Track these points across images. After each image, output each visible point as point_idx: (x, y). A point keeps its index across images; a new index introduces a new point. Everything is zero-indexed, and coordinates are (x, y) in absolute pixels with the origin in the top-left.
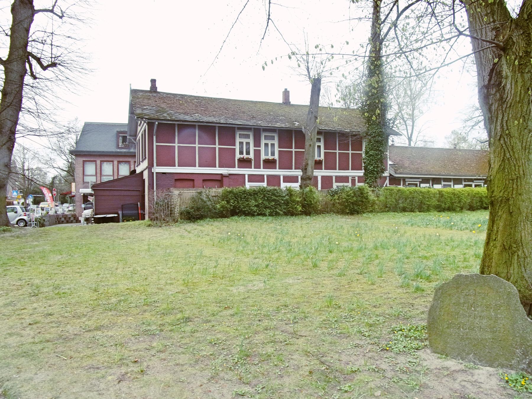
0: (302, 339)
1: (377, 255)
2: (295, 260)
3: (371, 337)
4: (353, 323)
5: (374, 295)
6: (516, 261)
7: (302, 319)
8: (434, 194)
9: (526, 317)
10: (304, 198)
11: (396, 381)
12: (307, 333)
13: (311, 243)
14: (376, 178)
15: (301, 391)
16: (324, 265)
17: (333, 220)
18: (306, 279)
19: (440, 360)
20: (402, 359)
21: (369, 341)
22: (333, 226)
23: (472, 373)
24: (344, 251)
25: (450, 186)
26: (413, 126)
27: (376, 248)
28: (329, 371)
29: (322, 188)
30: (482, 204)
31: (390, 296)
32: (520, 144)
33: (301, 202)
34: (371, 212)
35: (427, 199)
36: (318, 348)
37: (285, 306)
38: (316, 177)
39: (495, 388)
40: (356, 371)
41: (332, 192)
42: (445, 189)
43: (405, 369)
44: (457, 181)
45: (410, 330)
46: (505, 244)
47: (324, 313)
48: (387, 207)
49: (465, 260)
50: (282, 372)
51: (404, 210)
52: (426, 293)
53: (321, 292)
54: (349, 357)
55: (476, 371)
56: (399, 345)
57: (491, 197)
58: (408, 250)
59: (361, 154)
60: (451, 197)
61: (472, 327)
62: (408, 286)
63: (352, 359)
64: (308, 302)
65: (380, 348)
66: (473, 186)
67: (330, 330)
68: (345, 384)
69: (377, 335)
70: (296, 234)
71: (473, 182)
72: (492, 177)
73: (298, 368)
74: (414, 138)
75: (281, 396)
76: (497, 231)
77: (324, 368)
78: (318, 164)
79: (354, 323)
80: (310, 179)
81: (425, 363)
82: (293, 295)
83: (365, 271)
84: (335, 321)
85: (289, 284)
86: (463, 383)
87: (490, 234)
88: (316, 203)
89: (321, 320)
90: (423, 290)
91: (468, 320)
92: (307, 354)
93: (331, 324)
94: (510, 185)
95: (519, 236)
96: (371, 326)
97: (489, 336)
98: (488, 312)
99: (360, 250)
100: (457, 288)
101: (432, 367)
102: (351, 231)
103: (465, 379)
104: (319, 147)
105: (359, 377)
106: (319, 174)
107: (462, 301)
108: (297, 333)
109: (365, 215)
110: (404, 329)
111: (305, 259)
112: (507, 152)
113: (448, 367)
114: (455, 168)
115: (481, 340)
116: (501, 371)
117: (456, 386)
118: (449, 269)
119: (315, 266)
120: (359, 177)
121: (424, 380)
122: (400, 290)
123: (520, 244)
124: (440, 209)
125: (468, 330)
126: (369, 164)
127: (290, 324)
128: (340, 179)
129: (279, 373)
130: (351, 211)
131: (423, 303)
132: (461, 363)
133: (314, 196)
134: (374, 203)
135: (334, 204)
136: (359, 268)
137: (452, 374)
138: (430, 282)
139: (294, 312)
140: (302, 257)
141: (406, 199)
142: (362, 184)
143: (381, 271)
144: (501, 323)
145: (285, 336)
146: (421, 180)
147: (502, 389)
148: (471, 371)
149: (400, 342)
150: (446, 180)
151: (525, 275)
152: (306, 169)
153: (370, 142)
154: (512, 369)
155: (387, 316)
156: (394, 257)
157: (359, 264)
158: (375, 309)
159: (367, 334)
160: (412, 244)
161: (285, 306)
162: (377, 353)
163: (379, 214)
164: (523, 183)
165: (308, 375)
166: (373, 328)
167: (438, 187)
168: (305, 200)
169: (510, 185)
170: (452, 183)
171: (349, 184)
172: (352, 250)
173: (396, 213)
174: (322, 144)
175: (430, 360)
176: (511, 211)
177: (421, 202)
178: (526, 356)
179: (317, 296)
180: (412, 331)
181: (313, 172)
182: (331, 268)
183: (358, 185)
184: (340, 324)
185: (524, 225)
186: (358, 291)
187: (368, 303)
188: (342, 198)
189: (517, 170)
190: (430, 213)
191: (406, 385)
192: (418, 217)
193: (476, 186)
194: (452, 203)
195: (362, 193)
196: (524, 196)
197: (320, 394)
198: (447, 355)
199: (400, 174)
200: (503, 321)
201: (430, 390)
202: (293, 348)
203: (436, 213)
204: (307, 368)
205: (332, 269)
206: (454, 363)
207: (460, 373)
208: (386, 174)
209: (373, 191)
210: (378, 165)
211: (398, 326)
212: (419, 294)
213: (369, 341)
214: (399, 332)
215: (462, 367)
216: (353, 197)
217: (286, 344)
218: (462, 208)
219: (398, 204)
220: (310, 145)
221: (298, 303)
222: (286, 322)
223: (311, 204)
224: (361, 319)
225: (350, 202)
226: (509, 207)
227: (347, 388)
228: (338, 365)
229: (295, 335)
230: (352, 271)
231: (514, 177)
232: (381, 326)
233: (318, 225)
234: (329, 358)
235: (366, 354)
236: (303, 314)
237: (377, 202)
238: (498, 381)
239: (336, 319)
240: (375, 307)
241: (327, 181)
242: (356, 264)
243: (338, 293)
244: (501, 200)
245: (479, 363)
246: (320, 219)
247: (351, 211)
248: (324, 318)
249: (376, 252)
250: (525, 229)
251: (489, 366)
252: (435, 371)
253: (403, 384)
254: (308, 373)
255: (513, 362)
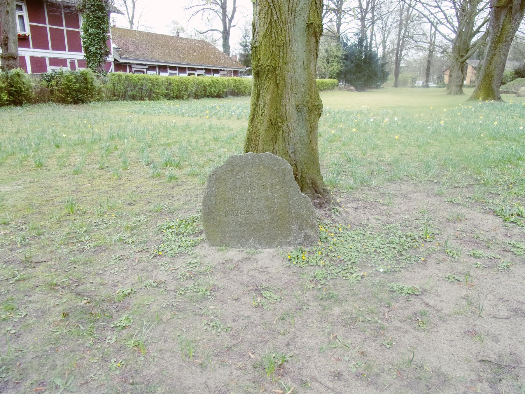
0: (41, 268)
1: (116, 146)
2: (9, 161)
3: (136, 243)
4: (109, 230)
5: (125, 191)
6: (281, 137)
7: (34, 238)
8: (163, 82)
9: (300, 192)
10: (10, 83)
11: (183, 293)
12: (48, 256)
13: (28, 138)
14: (100, 62)
15: (56, 350)
16: (52, 164)
17: (53, 110)
18: (30, 182)
19: (220, 253)
20: (180, 262)
21: (135, 249)
22: (54, 117)
23: (255, 259)
24: (75, 145)
25: (176, 74)
26: (134, 8)
27: (112, 138)
28: (92, 304)
29: (33, 71)
30: (206, 92)
31: (143, 189)
32: (287, 5)
33: (5, 89)
34: (99, 100)
35: (156, 87)
36: (68, 274)
37: (5, 224)
38: (23, 58)
39: (281, 269)
40: (129, 294)
41: (48, 76)
42: (172, 77)
43: (187, 273)
44: (182, 70)
45: (179, 226)
46: (272, 119)
47: (65, 224)
48: (115, 95)
49: (206, 144)
50: (18, 328)
51: (134, 98)
52: (181, 180)
53: (56, 196)
54: (115, 276)
55: (258, 256)
56: (173, 246)
57: (257, 67)
58: (148, 139)
59: (78, 33)
60: (178, 85)
61: (250, 211)
62: (159, 176)
63: (119, 278)
64: (38, 213)
65: (151, 255)
66: (196, 75)
67: (79, 245)
68: (120, 316)
69: (143, 239)
70: (5, 129)
71: (196, 71)
72: (257, 43)
73: (43, 313)
74: (135, 22)
75: (23, 369)
76: (264, 105)
77: (84, 302)
78: (23, 40)
79: (110, 230)
80: (15, 59)
81: (206, 261)
82: (14, 206)
83: (107, 164)
84: (84, 232)
85: (6, 193)
86: (251, 273)
87: (255, 109)
88: (28, 90)
89: (64, 233)
90: (177, 179)
91: (246, 204)
92: (53, 287)
93: (80, 237)
94: (277, 53)
95: (284, 110)
96: (132, 229)
97: (267, 217)
98: (265, 193)
99: (94, 142)
100: (233, 171)
101: (215, 263)
102: (78, 122)
103: (252, 268)
104: (21, 17)
105: (134, 301)
106: (28, 53)
107: (238, 185)
108: (30, 260)
109: (91, 104)
110: (173, 226)
111: (24, 159)
112: (274, 13)
113: (231, 258)
114: (179, 57)
115: (260, 223)
116: (281, 250)
117: (246, 278)
118: (194, 153)
119: (40, 165)
120: (79, 61)
121: (212, 281)
122: (152, 182)
123: (285, 118)
124: (169, 97)
125: (246, 215)
126: (90, 44)
127: (18, 248)
128: (54, 62)
129: (13, 331)
130: (75, 100)
131: (181, 192)
132: (242, 251)
133: (24, 81)
134: (100, 91)
135: (52, 92)
136: (98, 162)
137: (237, 267)
138: (181, 169)
139: (21, 230)
140: (19, 156)
141: (135, 87)
142: (82, 69)
143: (125, 162)
144: (277, 202)
145: (12, 268)
146: (147, 67)
147: (287, 269)
148: (254, 257)
149: (173, 243)
150: (172, 68)
151: (289, 151)
152: (6, 45)
153: (88, 16)
154: (290, 246)
155: (149, 214)
156: (135, 147)
157: (96, 158)
158: (130, 208)
159: (130, 240)
160: (151, 132)
161: (5, 224)
162: (149, 262)
163: (107, 103)
164: (289, 51)
165: (61, 321)
166: (135, 232)
167: (164, 75)
168: (12, 86)
169: (277, 53)
170: (177, 72)
171: (68, 68)
172: (85, 143)
173: (126, 102)
174: (25, 13)
175: (211, 255)
176: (278, 82)
177: (151, 90)
178: (301, 230)
179: (51, 203)
180: (182, 226)
181: (17, 51)
182: (61, 166)
183: (80, 70)
184: (92, 235)
185: (289, 97)
186: (104, 189)
187: (119, 201)
188: (61, 84)
189: (283, 35)
190: (160, 101)
191: (194, 294)
192: (147, 105)
193: (198, 75)
194: (180, 91)
195: (86, 79)
196: (290, 66)
197: (87, 345)
198: (226, 246)
199: (126, 59)
200: (280, 200)
201: (222, 292)
202: (29, 284)
203: (165, 101)
204: (58, 309)
205: (64, 166)
206: (235, 253)
207: (244, 262)
208: (110, 59)
209: (98, 76)
210: (101, 46)
211: (165, 223)
212: (173, 183)
213: (135, 249)
214: (168, 231)
215: (244, 255)
216: (75, 83)
217: (17, 281)
218: (189, 96)
219: (127, 92)
220: (8, 12)
221: (23, 217)
222: (10, 247)
223: (22, 91)
224: (117, 223)
225: (72, 88)
226: (276, 78)
227: (123, 324)
228: (104, 292)
229: (29, 263)
230: (90, 167)
231: (281, 43)
232: (144, 227)
233: (34, 117)
234: (88, 285)
235: (136, 267)
236: (36, 231)
237: (104, 89)
238: (281, 262)
239: (85, 229)
240: (130, 204)
241: (38, 64)
242: (93, 157)
243: (79, 195)
244: (269, 70)
245: (259, 247)
246: (36, 110)
247: (75, 100)
248: (68, 230)
249: (113, 143)
250: (289, 102)
251: (269, 248)
252: (219, 267)
253: (192, 294)
254: (61, 317)
255: (290, 238)
